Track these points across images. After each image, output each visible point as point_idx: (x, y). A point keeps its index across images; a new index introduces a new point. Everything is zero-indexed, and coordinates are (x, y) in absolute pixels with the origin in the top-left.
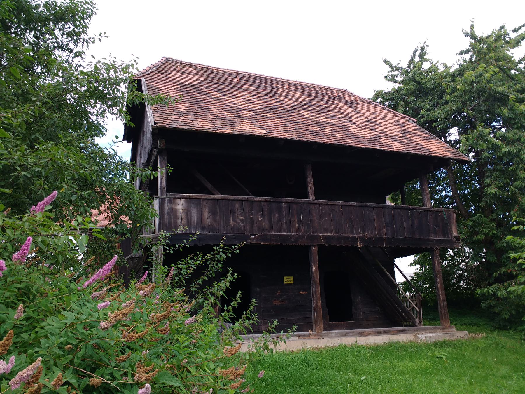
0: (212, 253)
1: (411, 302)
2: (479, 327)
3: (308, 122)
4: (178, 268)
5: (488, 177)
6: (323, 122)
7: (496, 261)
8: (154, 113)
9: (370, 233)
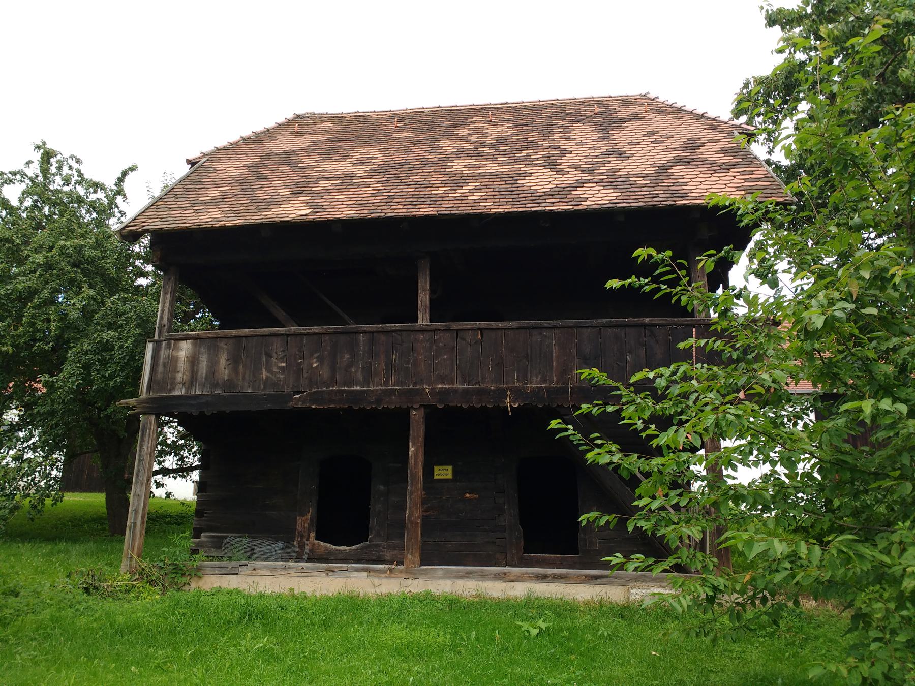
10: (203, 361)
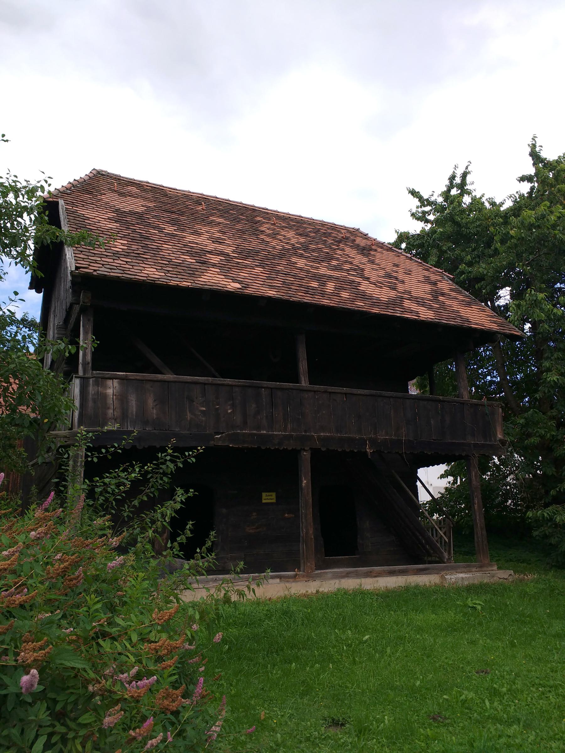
0: (155, 462)
1: (438, 529)
2: (530, 564)
3: (302, 274)
4: (105, 484)
5: (547, 358)
6: (324, 275)
7: (555, 473)
8: (76, 252)
9: (384, 433)
10: (132, 400)
